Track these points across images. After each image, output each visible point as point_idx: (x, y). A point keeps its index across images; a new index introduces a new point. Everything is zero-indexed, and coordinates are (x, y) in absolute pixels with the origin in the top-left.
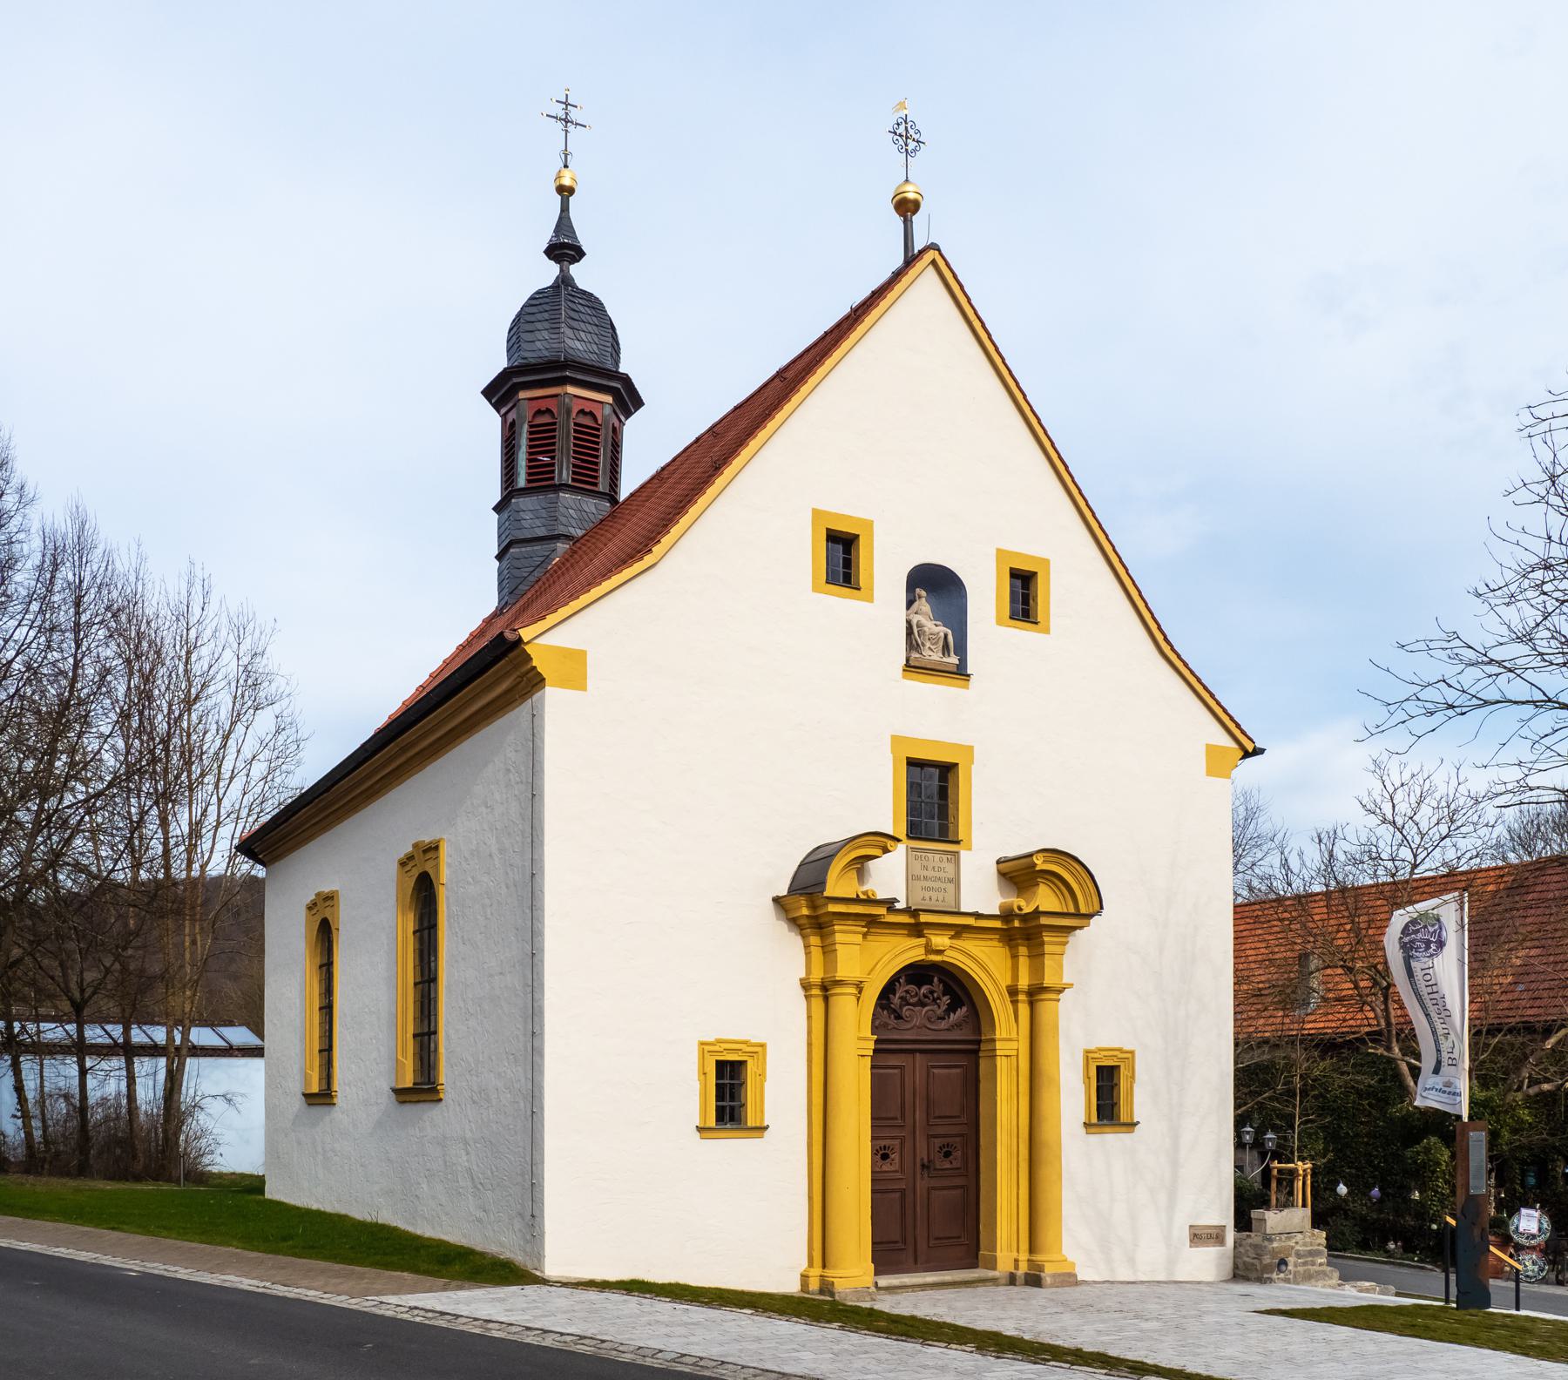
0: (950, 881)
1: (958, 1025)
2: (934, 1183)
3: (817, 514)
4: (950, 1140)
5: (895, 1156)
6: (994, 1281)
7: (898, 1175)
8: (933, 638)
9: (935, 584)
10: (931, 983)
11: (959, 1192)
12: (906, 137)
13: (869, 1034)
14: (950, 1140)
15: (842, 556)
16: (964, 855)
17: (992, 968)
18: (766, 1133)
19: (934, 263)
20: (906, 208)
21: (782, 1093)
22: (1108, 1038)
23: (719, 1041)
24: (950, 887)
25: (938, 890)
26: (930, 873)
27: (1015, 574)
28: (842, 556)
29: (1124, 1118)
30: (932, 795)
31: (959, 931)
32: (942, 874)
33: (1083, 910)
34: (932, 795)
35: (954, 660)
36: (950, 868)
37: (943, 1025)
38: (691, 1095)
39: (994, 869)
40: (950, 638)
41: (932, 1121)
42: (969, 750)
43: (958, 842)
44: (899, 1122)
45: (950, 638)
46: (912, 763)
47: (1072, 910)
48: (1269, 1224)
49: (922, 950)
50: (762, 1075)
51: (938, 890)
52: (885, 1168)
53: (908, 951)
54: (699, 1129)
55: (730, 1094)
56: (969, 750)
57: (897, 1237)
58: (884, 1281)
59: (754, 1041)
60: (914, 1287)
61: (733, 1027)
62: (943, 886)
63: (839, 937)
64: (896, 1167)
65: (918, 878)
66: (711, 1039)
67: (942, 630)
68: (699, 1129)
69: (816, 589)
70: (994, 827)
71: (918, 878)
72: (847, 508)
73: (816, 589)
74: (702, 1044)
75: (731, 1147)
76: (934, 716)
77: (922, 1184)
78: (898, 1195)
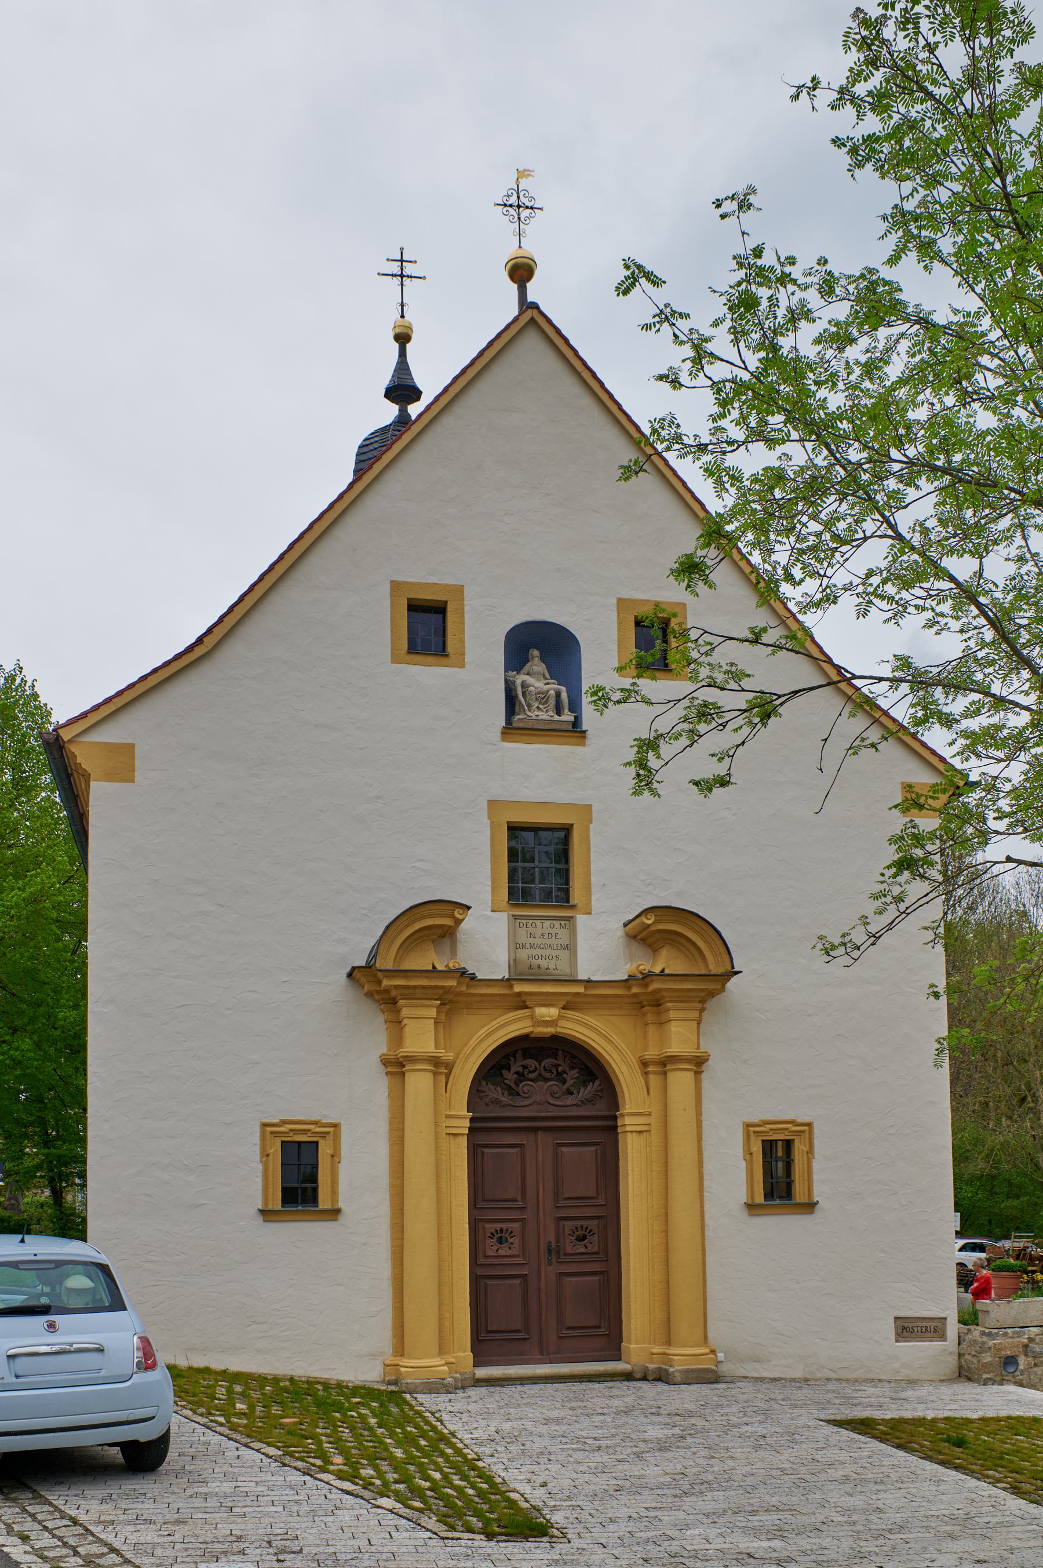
0: (565, 947)
1: (584, 1102)
2: (563, 1269)
3: (396, 587)
4: (504, 1226)
5: (516, 1241)
6: (628, 1376)
7: (520, 1260)
8: (543, 698)
9: (541, 644)
10: (555, 1056)
11: (597, 1278)
12: (518, 207)
13: (465, 1112)
14: (584, 1223)
15: (427, 625)
16: (581, 919)
17: (615, 1038)
18: (342, 1219)
19: (532, 320)
20: (521, 272)
21: (358, 1175)
22: (777, 1108)
23: (284, 1122)
24: (564, 954)
25: (549, 957)
26: (538, 941)
27: (415, 608)
28: (427, 625)
29: (799, 1194)
30: (540, 862)
31: (570, 1004)
32: (553, 941)
33: (714, 970)
34: (540, 862)
35: (568, 717)
36: (563, 935)
37: (570, 1100)
38: (253, 1179)
39: (621, 932)
40: (564, 695)
41: (561, 1203)
42: (587, 809)
43: (573, 907)
44: (520, 1204)
45: (564, 695)
46: (514, 830)
47: (703, 972)
48: (992, 1315)
49: (527, 1023)
50: (810, 1152)
51: (549, 957)
52: (502, 1252)
53: (513, 1026)
54: (262, 1212)
55: (299, 1180)
56: (587, 809)
57: (489, 1329)
58: (482, 1372)
59: (800, 1120)
60: (534, 1380)
61: (301, 1105)
62: (554, 953)
63: (405, 1012)
64: (569, 1250)
65: (524, 946)
66: (756, 1121)
67: (553, 687)
68: (262, 1212)
69: (395, 659)
70: (612, 892)
71: (524, 946)
72: (427, 575)
73: (395, 659)
74: (265, 1125)
75: (300, 1234)
76: (541, 778)
77: (549, 1272)
78: (517, 1281)
